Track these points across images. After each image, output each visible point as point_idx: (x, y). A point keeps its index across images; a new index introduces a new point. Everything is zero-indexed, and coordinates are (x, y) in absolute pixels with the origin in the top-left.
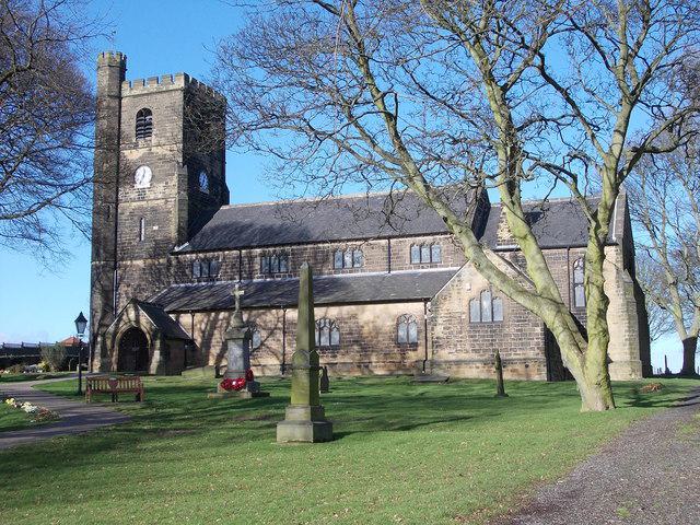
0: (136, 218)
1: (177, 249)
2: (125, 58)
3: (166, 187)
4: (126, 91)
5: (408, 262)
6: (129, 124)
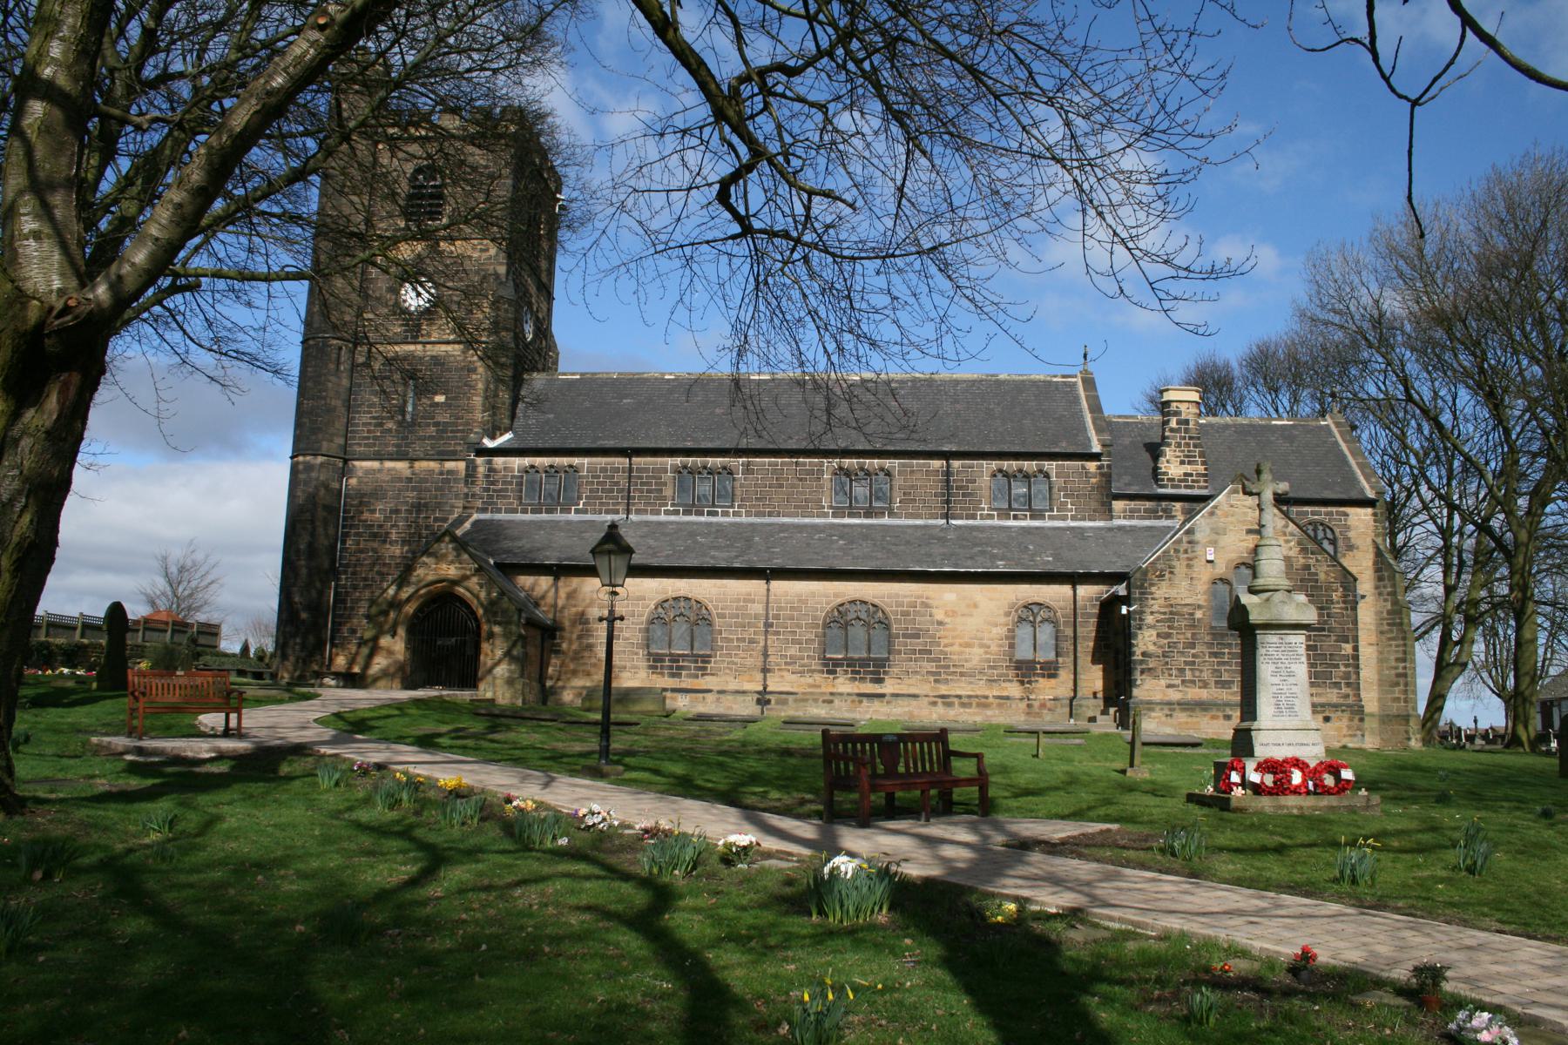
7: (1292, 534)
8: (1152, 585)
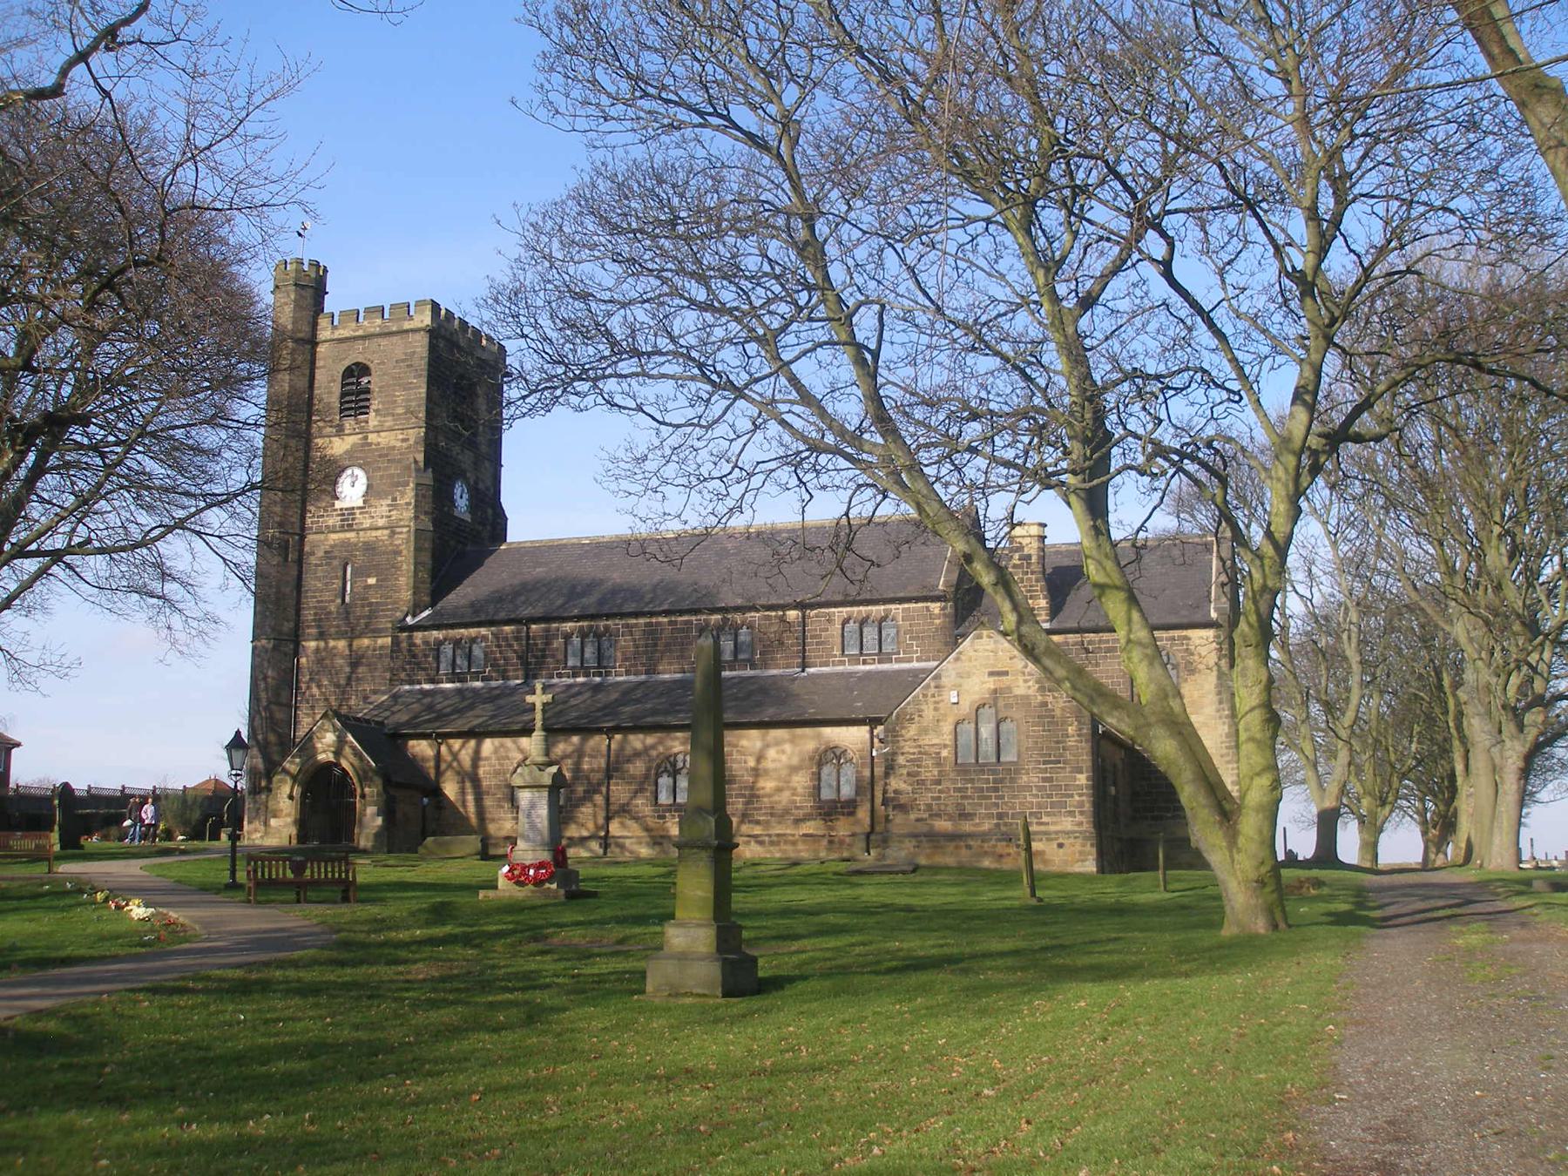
0: (336, 563)
1: (409, 620)
2: (325, 270)
3: (393, 507)
4: (324, 333)
5: (837, 652)
6: (328, 386)
7: (1030, 674)
8: (903, 728)
